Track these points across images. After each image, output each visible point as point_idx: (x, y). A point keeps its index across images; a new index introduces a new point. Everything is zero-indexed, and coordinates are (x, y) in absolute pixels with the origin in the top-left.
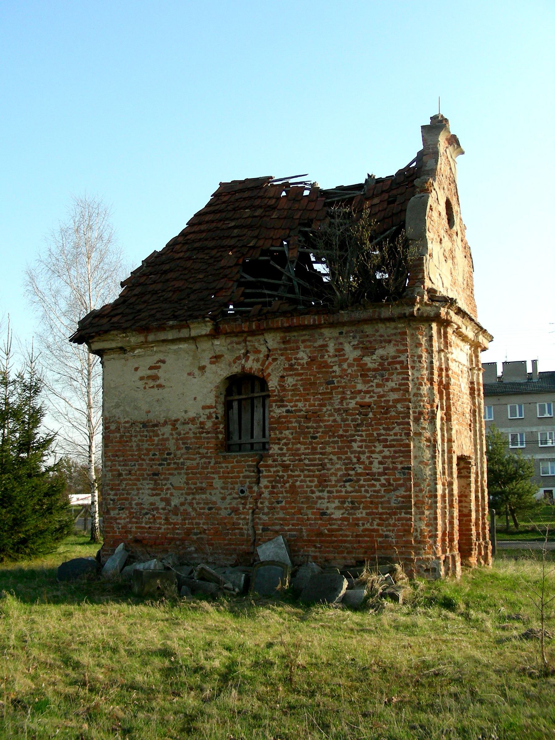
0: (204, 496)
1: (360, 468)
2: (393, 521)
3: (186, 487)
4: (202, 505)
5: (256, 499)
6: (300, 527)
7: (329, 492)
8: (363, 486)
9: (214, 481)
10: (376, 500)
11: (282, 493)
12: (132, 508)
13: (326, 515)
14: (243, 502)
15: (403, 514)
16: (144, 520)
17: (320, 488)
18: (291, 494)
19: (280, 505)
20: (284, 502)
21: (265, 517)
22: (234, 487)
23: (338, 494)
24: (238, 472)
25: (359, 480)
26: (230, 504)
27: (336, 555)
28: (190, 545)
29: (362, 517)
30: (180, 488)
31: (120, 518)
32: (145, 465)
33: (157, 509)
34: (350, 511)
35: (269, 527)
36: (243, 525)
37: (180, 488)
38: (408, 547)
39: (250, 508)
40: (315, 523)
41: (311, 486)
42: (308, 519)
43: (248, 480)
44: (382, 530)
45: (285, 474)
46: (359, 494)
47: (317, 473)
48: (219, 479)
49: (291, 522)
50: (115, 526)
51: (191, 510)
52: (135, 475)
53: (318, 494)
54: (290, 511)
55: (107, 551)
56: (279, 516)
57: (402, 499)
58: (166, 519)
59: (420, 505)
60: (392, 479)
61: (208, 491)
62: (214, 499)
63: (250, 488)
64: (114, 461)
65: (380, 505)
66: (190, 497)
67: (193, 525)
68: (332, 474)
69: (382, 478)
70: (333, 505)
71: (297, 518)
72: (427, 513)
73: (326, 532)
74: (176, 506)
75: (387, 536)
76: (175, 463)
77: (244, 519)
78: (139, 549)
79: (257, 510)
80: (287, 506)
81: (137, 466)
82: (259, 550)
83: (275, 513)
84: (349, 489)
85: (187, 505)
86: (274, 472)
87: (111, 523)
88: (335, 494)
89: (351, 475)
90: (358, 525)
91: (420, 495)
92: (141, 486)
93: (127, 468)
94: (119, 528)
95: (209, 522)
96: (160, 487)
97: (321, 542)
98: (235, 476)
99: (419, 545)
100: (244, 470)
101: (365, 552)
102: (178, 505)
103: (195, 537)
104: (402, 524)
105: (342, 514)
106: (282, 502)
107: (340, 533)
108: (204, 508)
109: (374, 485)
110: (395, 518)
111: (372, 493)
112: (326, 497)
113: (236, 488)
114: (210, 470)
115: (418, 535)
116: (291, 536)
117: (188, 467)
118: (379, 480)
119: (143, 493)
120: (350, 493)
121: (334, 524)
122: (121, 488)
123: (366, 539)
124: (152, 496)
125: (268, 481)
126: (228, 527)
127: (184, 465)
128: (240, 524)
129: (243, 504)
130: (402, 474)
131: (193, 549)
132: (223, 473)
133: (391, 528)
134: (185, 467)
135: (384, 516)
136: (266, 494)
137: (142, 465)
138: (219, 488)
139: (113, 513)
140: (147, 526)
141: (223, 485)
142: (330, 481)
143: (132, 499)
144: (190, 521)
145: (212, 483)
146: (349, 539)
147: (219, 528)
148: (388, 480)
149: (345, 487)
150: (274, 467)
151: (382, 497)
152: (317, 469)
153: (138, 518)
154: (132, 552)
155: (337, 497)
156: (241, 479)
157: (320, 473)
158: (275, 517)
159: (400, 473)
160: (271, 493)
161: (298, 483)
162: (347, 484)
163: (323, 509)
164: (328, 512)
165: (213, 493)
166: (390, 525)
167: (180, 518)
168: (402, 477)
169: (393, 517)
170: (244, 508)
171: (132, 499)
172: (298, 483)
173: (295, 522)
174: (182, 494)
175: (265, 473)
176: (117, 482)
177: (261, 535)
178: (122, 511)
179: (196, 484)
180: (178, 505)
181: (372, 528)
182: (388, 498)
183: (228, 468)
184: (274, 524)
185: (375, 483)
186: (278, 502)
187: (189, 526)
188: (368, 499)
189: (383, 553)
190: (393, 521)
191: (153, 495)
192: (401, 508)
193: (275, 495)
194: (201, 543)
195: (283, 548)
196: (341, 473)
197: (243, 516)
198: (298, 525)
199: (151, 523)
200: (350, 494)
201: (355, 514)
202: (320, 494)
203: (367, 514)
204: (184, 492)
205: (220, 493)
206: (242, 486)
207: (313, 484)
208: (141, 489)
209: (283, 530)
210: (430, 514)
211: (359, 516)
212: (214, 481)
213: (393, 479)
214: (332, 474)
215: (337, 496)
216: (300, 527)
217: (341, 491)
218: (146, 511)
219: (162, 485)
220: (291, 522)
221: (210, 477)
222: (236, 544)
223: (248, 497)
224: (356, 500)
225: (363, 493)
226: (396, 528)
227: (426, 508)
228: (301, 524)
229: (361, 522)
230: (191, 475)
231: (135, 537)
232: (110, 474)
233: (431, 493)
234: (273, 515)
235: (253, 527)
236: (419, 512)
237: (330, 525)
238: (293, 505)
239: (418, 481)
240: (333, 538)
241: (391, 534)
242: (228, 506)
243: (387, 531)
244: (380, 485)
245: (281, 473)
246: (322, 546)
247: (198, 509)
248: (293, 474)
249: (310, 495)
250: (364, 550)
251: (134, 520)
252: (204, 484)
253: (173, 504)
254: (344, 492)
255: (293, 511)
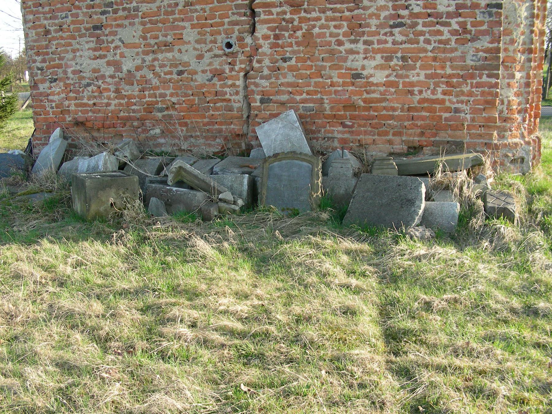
0: (169, 55)
1: (418, 5)
2: (469, 88)
3: (143, 42)
4: (167, 69)
5: (251, 56)
6: (319, 96)
7: (366, 43)
8: (422, 33)
9: (184, 32)
10: (443, 55)
11: (291, 45)
12: (68, 78)
13: (361, 78)
14: (230, 60)
15: (485, 76)
16: (85, 94)
17: (353, 37)
18: (306, 47)
19: (288, 63)
20: (294, 59)
21: (265, 83)
22: (215, 39)
23: (381, 46)
24: (221, 17)
25: (417, 24)
26: (210, 64)
27: (376, 137)
28: (154, 125)
29: (418, 82)
30: (134, 46)
31: (53, 94)
32: (81, 14)
33: (103, 77)
34: (400, 72)
35: (271, 97)
36: (231, 95)
37: (134, 46)
38: (489, 127)
39: (241, 70)
40: (344, 90)
41: (338, 35)
42: (333, 84)
43: (237, 27)
44: (449, 100)
45: (295, 17)
46: (416, 45)
47: (347, 14)
48: (192, 28)
49: (306, 89)
50: (47, 104)
51: (152, 76)
52: (69, 31)
53: (348, 46)
54: (304, 72)
55: (40, 139)
56: (286, 80)
57: (485, 55)
58: (117, 91)
59: (509, 64)
60: (469, 23)
61: (176, 48)
62: (185, 58)
63: (241, 39)
64: (38, 12)
65: (448, 63)
66: (149, 58)
67: (156, 97)
68: (371, 16)
69: (453, 21)
70: (373, 63)
71: (315, 82)
72: (518, 75)
73: (362, 104)
74: (129, 71)
75: (457, 110)
76: (124, 9)
77: (233, 85)
78: (81, 135)
79: (252, 72)
80: (299, 64)
81: (70, 17)
82: (260, 132)
83: (280, 77)
84: (399, 38)
85: (145, 69)
86: (278, 14)
87: (41, 101)
88: (376, 46)
89: (403, 17)
90: (411, 93)
91: (511, 48)
92: (78, 46)
93: (57, 21)
94: (52, 108)
95: (179, 92)
96: (105, 45)
97: (352, 118)
98: (216, 23)
99: (504, 124)
100: (230, 12)
101: (422, 134)
102: (133, 70)
103: (160, 115)
104: (483, 93)
105: (387, 77)
106: (291, 59)
107: (384, 104)
108: (171, 73)
109: (440, 33)
110: (472, 83)
111: (436, 45)
112: (362, 51)
113: (219, 41)
114: (177, 16)
115: (505, 109)
116: (305, 109)
117: (144, 14)
118: (448, 24)
119: (81, 56)
120: (401, 44)
121: (374, 92)
122: (50, 50)
123: (424, 114)
124: (94, 59)
125: (268, 28)
126: (208, 99)
127: (138, 11)
128: (226, 93)
129: (230, 63)
130: (486, 15)
131: (158, 131)
132: (198, 18)
133: (465, 98)
134: (140, 14)
135: (455, 80)
136: (266, 48)
137: (77, 15)
138: (192, 42)
139: (42, 87)
140: (91, 102)
141: (199, 37)
142: (368, 26)
143: (67, 66)
144: (152, 92)
145: (182, 34)
146: (397, 113)
147: (194, 100)
148: (463, 25)
149: (392, 34)
150: (277, 7)
151: (455, 50)
152: (347, 8)
153: (77, 92)
154: (73, 140)
155: (379, 51)
156: (226, 26)
157: (352, 13)
158: (279, 82)
159: (484, 13)
160: (274, 46)
161: (316, 30)
162: (396, 30)
163: (357, 69)
164: (365, 73)
165: (183, 51)
166: (462, 93)
167: (136, 88)
168: (487, 19)
169: (469, 81)
170: (232, 70)
171: (67, 66)
172: (316, 30)
173: (312, 88)
174: (137, 54)
175: (263, 17)
176: (44, 43)
177: (258, 109)
178: (54, 84)
179: (156, 37)
180: (133, 70)
181: (434, 97)
182: (462, 53)
183: (205, 12)
184: (278, 93)
185: (442, 28)
186: (285, 60)
187: (151, 99)
188: (430, 54)
189: (449, 136)
190: (469, 88)
191: (96, 58)
192: (482, 68)
193: (280, 49)
194: (170, 123)
195: (297, 128)
196: (387, 13)
197: (230, 82)
198: (316, 92)
199: (95, 97)
200: (401, 46)
201: (407, 76)
202: (353, 46)
203: (427, 76)
204: (140, 50)
205: (195, 49)
206: (227, 38)
207: (340, 31)
208: (78, 50)
209: (293, 101)
210: (521, 77)
211: (415, 79)
212: (184, 32)
213: (471, 22)
214: (371, 16)
215: (379, 49)
216: (319, 96)
217: (386, 42)
218: (87, 81)
219: (108, 42)
220: (306, 89)
221: (178, 26)
222: (221, 124)
223: (237, 52)
224: (410, 55)
225: (422, 44)
226: (472, 99)
227: (517, 69)
228: (321, 92)
229: (416, 89)
230: (149, 26)
231: (74, 118)
232: (34, 32)
233: (524, 46)
234: (277, 78)
235: (246, 97)
236: (508, 74)
237: (368, 93)
238: (309, 63)
239: (510, 26)
240: (372, 113)
241: (463, 107)
242: (208, 68)
243: (458, 102)
244: (449, 31)
245: (288, 16)
246: (354, 123)
247: (162, 74)
248: (309, 16)
249: (336, 47)
250: (419, 130)
251: (72, 95)
252: (169, 37)
253: (125, 69)
254: (390, 42)
255: (308, 72)
